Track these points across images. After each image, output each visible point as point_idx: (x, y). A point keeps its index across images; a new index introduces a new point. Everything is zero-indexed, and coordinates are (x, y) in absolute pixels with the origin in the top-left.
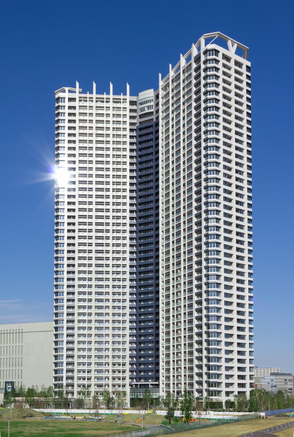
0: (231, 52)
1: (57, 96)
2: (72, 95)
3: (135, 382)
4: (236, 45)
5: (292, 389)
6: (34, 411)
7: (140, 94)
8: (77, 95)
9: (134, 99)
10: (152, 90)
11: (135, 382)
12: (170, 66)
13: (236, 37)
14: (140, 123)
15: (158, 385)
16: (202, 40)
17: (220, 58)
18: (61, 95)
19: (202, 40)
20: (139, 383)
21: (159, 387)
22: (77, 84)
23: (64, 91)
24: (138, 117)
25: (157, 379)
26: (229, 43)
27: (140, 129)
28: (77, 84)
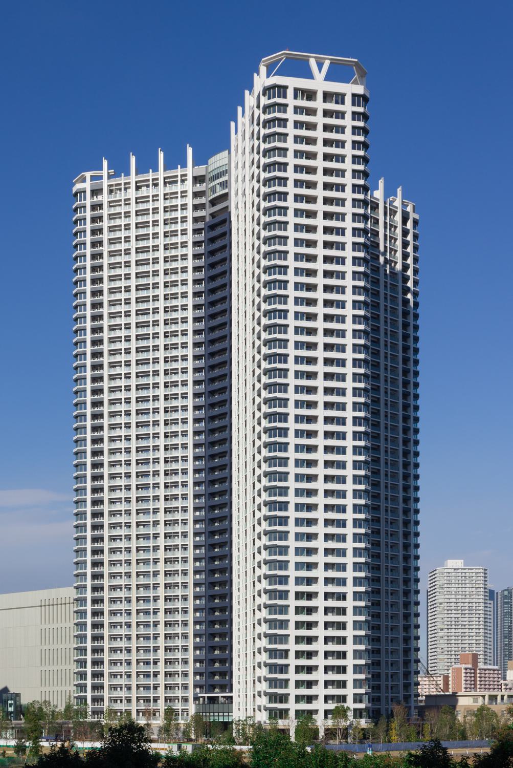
0: (319, 83)
1: (74, 190)
4: (327, 64)
7: (210, 161)
14: (213, 215)
15: (231, 697)
16: (263, 69)
18: (78, 186)
19: (263, 69)
22: (105, 163)
28: (105, 163)
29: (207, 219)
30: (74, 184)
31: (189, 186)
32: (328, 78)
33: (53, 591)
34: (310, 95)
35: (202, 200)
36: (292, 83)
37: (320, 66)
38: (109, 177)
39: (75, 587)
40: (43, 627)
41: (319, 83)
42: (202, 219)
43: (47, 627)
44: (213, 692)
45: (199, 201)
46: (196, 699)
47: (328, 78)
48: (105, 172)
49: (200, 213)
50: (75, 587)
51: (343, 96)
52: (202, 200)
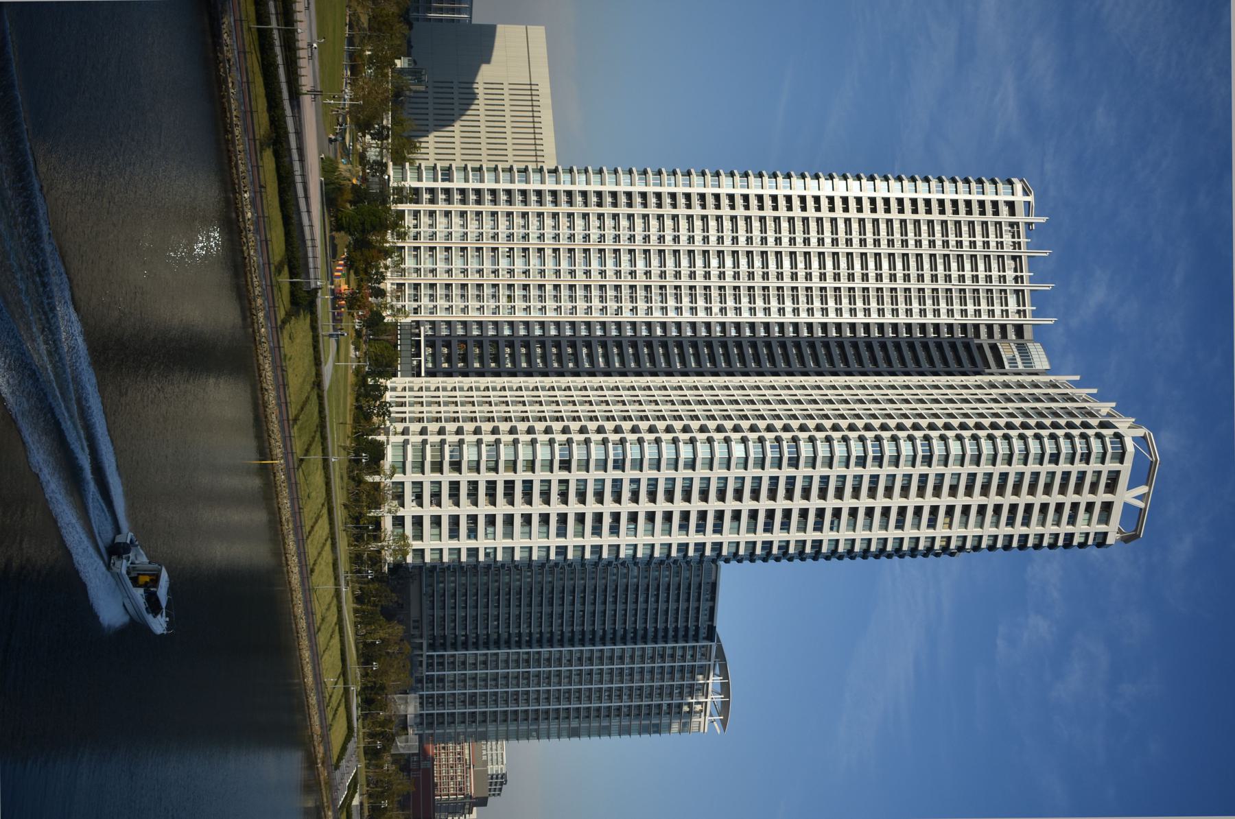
0: (1126, 496)
1: (1015, 180)
2: (1019, 209)
3: (424, 331)
4: (1141, 504)
5: (421, 697)
6: (330, 387)
7: (1038, 345)
8: (1020, 218)
9: (1028, 334)
10: (1046, 365)
11: (424, 331)
12: (1095, 391)
13: (1158, 500)
14: (980, 347)
15: (419, 375)
16: (1141, 432)
17: (1111, 465)
18: (1018, 187)
19: (1141, 432)
20: (422, 339)
21: (413, 376)
22: (1042, 220)
23: (1026, 193)
24: (992, 341)
25: (431, 373)
26: (1143, 489)
27: (967, 346)
28: (1042, 220)
29: (977, 341)
30: (1021, 180)
31: (1014, 319)
32: (1126, 505)
33: (549, 101)
34: (1111, 487)
35: (997, 335)
36: (1126, 469)
37: (1140, 498)
38: (1028, 224)
39: (411, 28)
40: (506, 86)
41: (1126, 496)
42: (977, 335)
43: (506, 92)
44: (426, 346)
45: (997, 330)
46: (418, 324)
47: (1126, 505)
48: (1032, 219)
49: (983, 331)
50: (411, 28)
51: (1107, 523)
52: (997, 335)
